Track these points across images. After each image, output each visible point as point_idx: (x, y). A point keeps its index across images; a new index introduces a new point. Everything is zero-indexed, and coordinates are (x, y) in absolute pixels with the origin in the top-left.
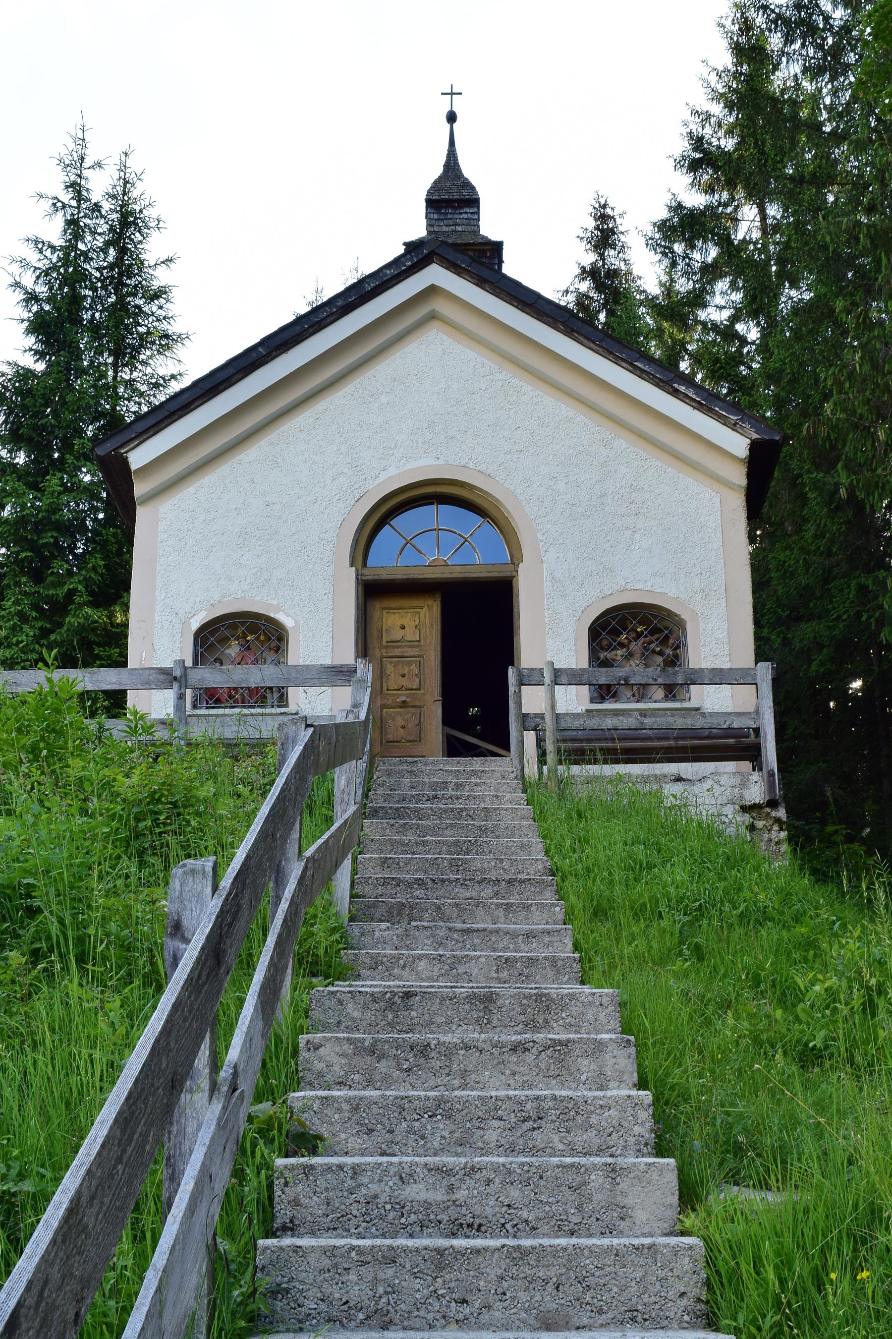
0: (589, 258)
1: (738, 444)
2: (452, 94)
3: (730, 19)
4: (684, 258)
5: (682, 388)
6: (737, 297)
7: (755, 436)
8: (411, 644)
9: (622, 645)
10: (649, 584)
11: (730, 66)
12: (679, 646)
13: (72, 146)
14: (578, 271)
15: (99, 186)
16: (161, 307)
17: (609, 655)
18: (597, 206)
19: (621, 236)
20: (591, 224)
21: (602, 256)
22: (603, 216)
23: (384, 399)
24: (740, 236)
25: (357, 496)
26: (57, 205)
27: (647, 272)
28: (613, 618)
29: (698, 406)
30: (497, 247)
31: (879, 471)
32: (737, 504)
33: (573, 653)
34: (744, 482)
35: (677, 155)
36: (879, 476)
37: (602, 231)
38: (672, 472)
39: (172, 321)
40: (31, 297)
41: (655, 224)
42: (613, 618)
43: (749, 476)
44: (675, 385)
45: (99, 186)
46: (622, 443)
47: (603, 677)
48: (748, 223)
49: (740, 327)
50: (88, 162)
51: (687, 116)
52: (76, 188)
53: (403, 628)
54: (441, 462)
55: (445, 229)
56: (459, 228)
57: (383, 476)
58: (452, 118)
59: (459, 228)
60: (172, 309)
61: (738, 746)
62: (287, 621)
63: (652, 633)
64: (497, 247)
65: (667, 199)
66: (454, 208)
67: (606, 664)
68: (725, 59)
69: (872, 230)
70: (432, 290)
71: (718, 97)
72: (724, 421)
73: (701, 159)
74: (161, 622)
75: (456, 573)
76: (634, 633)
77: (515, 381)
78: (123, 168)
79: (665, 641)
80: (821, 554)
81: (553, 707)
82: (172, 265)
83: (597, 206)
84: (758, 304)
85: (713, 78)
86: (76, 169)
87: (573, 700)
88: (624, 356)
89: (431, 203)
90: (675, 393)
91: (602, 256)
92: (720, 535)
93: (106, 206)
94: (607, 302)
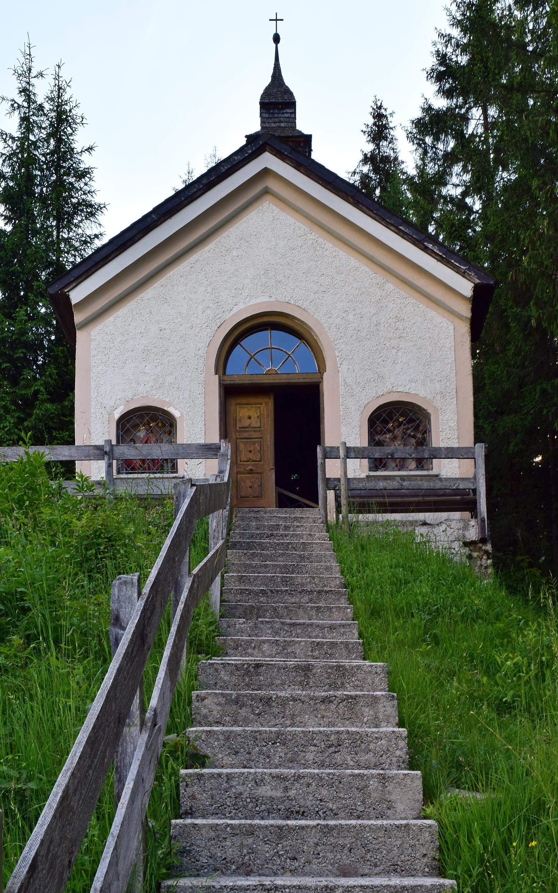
0: (369, 148)
1: (466, 287)
2: (276, 20)
4: (432, 148)
5: (430, 246)
6: (467, 177)
7: (477, 281)
9: (389, 431)
10: (407, 388)
12: (426, 431)
14: (361, 157)
15: (42, 91)
16: (86, 184)
18: (375, 107)
19: (391, 130)
20: (371, 121)
21: (378, 146)
22: (379, 115)
23: (235, 253)
25: (219, 324)
27: (408, 158)
29: (441, 259)
30: (308, 138)
33: (358, 438)
34: (469, 314)
41: (413, 122)
43: (473, 310)
45: (42, 91)
46: (391, 286)
49: (468, 200)
50: (34, 73)
51: (436, 38)
52: (26, 92)
54: (273, 299)
55: (273, 125)
56: (282, 125)
58: (276, 39)
59: (282, 125)
60: (94, 185)
61: (457, 500)
62: (176, 413)
64: (308, 138)
66: (279, 109)
67: (379, 444)
70: (266, 172)
72: (457, 270)
73: (445, 73)
75: (283, 379)
76: (398, 423)
77: (321, 240)
78: (57, 77)
79: (416, 429)
82: (92, 152)
83: (375, 107)
88: (392, 222)
90: (425, 249)
91: (378, 146)
93: (47, 106)
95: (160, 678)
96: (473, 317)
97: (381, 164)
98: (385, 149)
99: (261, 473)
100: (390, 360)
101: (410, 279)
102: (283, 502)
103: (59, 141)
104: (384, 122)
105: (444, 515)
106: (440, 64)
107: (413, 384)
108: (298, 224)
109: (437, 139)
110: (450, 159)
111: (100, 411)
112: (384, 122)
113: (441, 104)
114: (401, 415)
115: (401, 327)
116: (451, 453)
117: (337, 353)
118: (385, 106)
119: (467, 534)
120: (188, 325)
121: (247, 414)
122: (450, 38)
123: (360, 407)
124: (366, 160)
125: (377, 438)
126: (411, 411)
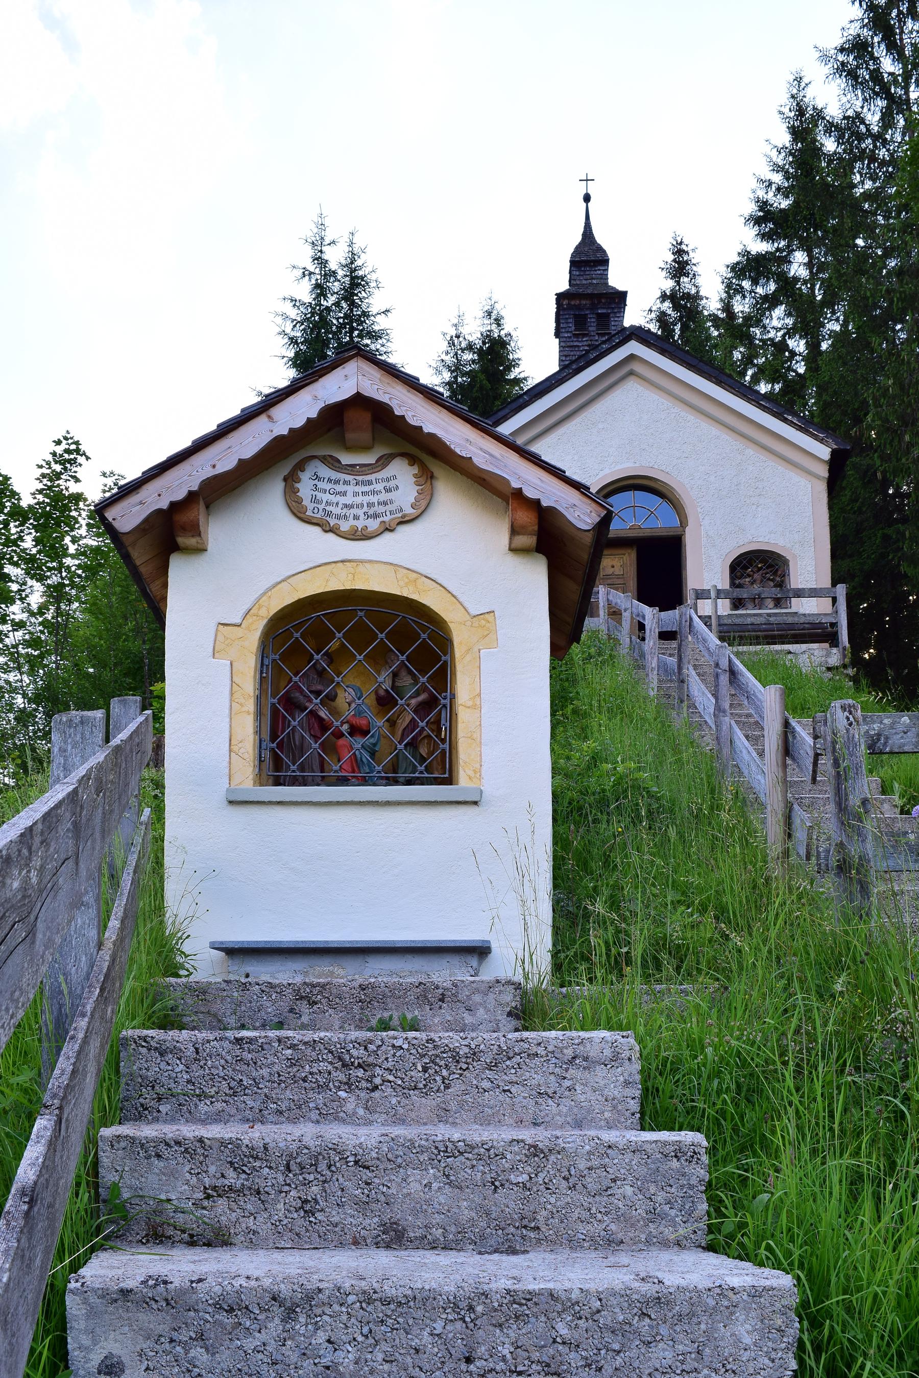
0: (668, 285)
1: (824, 452)
2: (587, 180)
3: (788, 107)
4: (751, 292)
5: (790, 418)
6: (790, 321)
8: (618, 577)
9: (749, 576)
11: (788, 145)
12: (785, 575)
13: (316, 230)
14: (659, 294)
15: (335, 257)
16: (383, 346)
17: (742, 581)
18: (675, 243)
19: (694, 267)
20: (670, 257)
21: (678, 283)
22: (679, 251)
24: (792, 274)
26: (307, 273)
27: (711, 291)
28: (745, 559)
29: (800, 429)
30: (623, 296)
31: (904, 460)
32: (822, 489)
33: (723, 581)
34: (826, 475)
35: (747, 215)
36: (903, 464)
37: (679, 263)
38: (781, 469)
39: (390, 355)
40: (293, 341)
41: (728, 266)
42: (745, 559)
45: (335, 257)
46: (751, 452)
47: (738, 593)
48: (798, 265)
49: (791, 343)
50: (327, 241)
51: (754, 184)
52: (320, 260)
53: (613, 567)
55: (584, 282)
56: (595, 281)
57: (601, 474)
58: (587, 198)
59: (595, 281)
60: (391, 346)
61: (823, 634)
63: (767, 568)
64: (623, 296)
65: (739, 248)
66: (590, 266)
67: (740, 586)
68: (786, 139)
69: (903, 295)
70: (632, 357)
71: (777, 168)
72: (816, 438)
73: (766, 219)
75: (647, 533)
76: (758, 569)
77: (683, 414)
78: (351, 244)
79: (775, 573)
80: (854, 513)
81: (716, 612)
82: (389, 314)
83: (675, 243)
84: (807, 324)
85: (774, 153)
86: (318, 245)
87: (724, 607)
88: (753, 398)
89: (573, 263)
90: (785, 420)
91: (678, 283)
93: (341, 273)
94: (681, 317)
97: (684, 303)
98: (687, 285)
101: (784, 453)
102: (660, 633)
103: (352, 304)
104: (685, 259)
105: (804, 647)
106: (760, 211)
108: (662, 400)
109: (755, 282)
110: (771, 301)
112: (685, 259)
113: (761, 247)
114: (760, 562)
116: (814, 593)
117: (699, 510)
118: (685, 241)
119: (829, 660)
121: (611, 564)
122: (770, 184)
124: (664, 297)
125: (737, 582)
126: (770, 558)
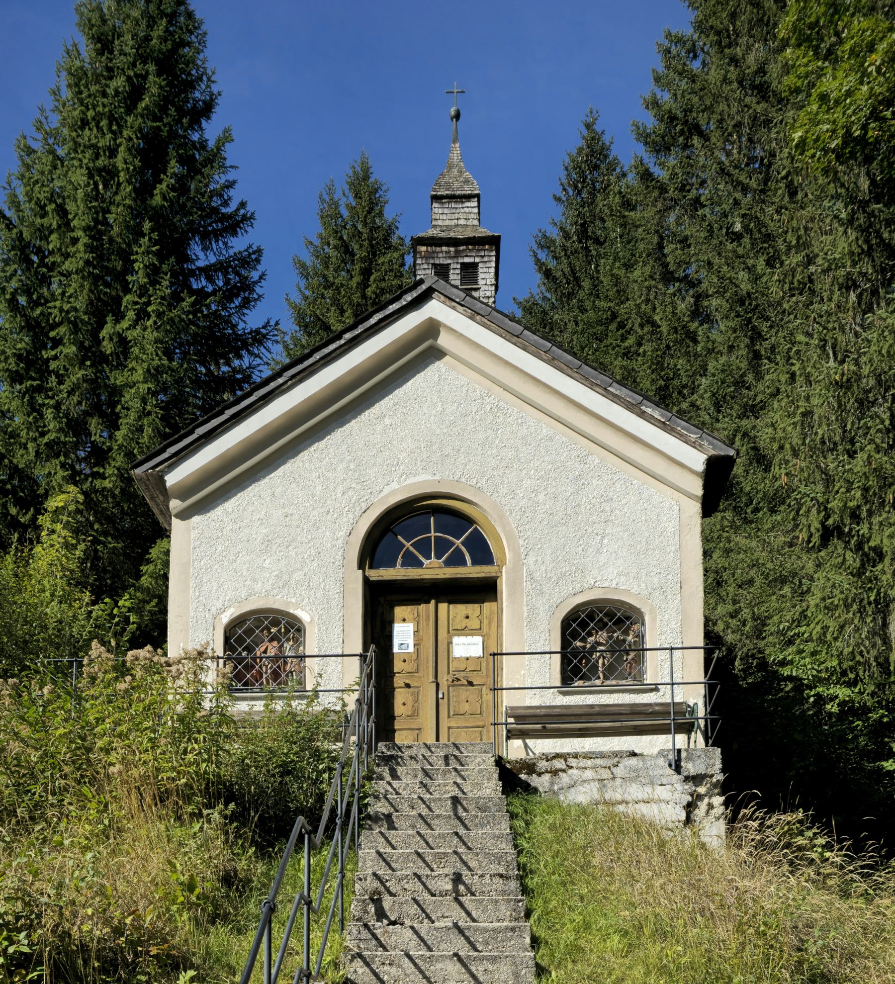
1: (698, 460)
5: (649, 411)
7: (713, 452)
10: (614, 582)
23: (387, 421)
25: (364, 508)
34: (700, 492)
43: (705, 487)
44: (643, 408)
54: (437, 477)
61: (675, 719)
62: (304, 615)
70: (432, 329)
74: (195, 620)
90: (642, 415)
92: (677, 539)
95: (562, 745)
96: (704, 496)
99: (418, 687)
100: (591, 550)
107: (623, 579)
111: (203, 614)
115: (608, 508)
120: (322, 510)
123: (550, 607)
